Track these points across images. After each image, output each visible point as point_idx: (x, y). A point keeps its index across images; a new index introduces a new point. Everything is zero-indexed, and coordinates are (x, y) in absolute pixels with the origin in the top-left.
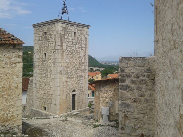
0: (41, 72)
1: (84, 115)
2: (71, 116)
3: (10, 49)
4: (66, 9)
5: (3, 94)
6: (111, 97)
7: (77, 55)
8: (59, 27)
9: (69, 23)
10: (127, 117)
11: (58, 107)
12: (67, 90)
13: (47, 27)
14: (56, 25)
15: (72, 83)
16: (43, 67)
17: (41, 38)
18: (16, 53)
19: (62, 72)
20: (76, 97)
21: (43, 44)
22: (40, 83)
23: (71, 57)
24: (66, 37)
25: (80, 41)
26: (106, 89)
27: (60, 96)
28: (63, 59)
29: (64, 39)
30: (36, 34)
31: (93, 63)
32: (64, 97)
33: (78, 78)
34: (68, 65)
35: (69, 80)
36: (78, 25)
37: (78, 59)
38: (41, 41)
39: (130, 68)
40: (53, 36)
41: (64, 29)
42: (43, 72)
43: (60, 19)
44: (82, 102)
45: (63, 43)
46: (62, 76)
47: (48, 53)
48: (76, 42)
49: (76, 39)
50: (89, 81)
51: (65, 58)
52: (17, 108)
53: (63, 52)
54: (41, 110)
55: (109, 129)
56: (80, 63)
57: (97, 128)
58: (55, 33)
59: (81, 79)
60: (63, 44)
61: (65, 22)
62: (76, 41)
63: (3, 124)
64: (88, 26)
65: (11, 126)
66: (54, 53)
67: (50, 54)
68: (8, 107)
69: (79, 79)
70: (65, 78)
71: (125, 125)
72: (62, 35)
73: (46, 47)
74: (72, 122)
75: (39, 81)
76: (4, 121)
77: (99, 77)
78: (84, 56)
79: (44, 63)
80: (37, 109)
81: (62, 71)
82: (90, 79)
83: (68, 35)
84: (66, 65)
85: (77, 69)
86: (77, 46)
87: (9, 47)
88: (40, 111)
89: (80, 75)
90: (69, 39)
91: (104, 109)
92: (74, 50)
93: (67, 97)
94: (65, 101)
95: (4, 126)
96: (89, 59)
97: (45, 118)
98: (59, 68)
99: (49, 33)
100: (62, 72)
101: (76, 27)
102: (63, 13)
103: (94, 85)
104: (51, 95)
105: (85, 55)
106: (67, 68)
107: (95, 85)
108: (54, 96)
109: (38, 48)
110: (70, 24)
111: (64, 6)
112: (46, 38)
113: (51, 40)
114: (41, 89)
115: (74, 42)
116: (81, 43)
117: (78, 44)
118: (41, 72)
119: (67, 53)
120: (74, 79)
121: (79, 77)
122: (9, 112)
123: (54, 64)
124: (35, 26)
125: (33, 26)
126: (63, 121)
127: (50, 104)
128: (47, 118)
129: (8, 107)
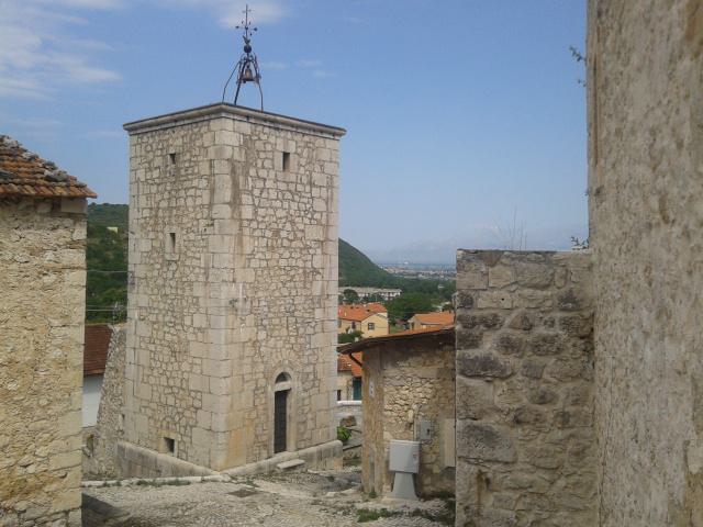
7: (295, 238)
13: (182, 133)
15: (275, 347)
16: (164, 286)
17: (156, 174)
20: (291, 401)
22: (152, 347)
24: (252, 172)
28: (242, 255)
35: (262, 335)
38: (159, 185)
40: (204, 169)
44: (314, 419)
48: (290, 191)
51: (248, 250)
56: (304, 272)
60: (240, 199)
66: (207, 232)
69: (301, 331)
70: (249, 329)
73: (178, 208)
83: (260, 165)
85: (294, 293)
86: (294, 206)
92: (284, 220)
95: (14, 510)
99: (188, 157)
104: (193, 394)
113: (195, 183)
115: (281, 191)
120: (284, 332)
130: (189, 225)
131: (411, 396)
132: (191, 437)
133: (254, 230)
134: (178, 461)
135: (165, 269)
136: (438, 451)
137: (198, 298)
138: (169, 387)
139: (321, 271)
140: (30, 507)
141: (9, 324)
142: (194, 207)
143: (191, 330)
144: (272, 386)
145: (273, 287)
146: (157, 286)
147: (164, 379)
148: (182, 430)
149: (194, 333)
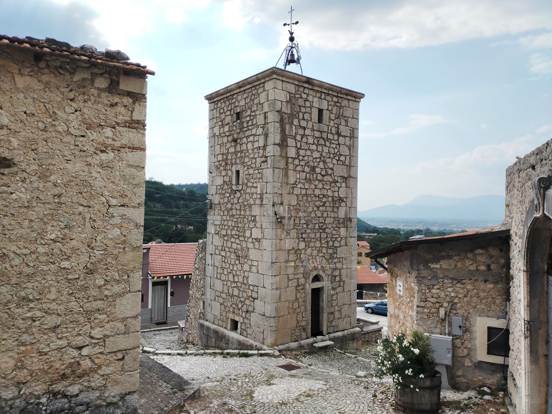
0: (226, 223)
7: (327, 174)
12: (297, 274)
13: (245, 96)
15: (311, 255)
16: (231, 209)
17: (226, 128)
19: (283, 221)
20: (325, 297)
22: (223, 253)
24: (296, 122)
28: (288, 184)
29: (291, 127)
30: (215, 120)
32: (290, 294)
34: (301, 203)
35: (302, 245)
37: (328, 187)
38: (228, 136)
40: (260, 120)
42: (232, 221)
44: (340, 311)
45: (289, 140)
46: (285, 233)
47: (246, 168)
48: (323, 139)
51: (292, 180)
52: (120, 326)
56: (333, 200)
59: (337, 244)
60: (287, 142)
66: (262, 167)
67: (251, 171)
69: (331, 243)
70: (292, 240)
72: (287, 116)
73: (241, 152)
75: (220, 248)
79: (234, 197)
83: (301, 117)
84: (294, 202)
85: (325, 215)
86: (326, 150)
88: (222, 330)
89: (334, 232)
92: (318, 160)
93: (299, 295)
94: (291, 306)
95: (65, 396)
99: (249, 112)
104: (251, 288)
111: (290, 44)
113: (254, 132)
114: (225, 271)
115: (316, 138)
116: (337, 142)
117: (328, 144)
118: (226, 223)
119: (299, 168)
120: (318, 244)
122: (88, 341)
130: (250, 163)
131: (442, 295)
132: (250, 320)
133: (297, 166)
134: (241, 338)
135: (232, 197)
136: (469, 346)
137: (255, 216)
138: (235, 282)
139: (345, 199)
140: (81, 391)
141: (63, 199)
142: (253, 150)
143: (250, 240)
144: (309, 284)
145: (310, 209)
146: (226, 209)
147: (231, 276)
148: (244, 314)
149: (253, 243)
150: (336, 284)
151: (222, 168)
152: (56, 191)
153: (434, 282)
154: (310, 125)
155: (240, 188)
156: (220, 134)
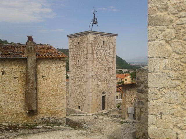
0: (75, 76)
1: (113, 115)
2: (101, 115)
3: (57, 61)
4: (95, 20)
5: (53, 94)
6: (135, 98)
8: (91, 38)
9: (99, 34)
10: (142, 111)
11: (90, 106)
14: (88, 36)
17: (75, 47)
18: (61, 64)
19: (93, 76)
20: (106, 98)
21: (77, 52)
22: (74, 86)
23: (101, 63)
24: (96, 46)
25: (109, 49)
26: (131, 91)
27: (92, 97)
28: (94, 65)
29: (95, 48)
31: (121, 64)
32: (96, 98)
33: (107, 82)
34: (98, 70)
35: (99, 83)
36: (106, 35)
38: (75, 49)
39: (143, 77)
40: (85, 46)
41: (95, 39)
43: (91, 31)
45: (94, 52)
48: (105, 50)
49: (105, 47)
50: (118, 83)
51: (95, 64)
52: (62, 105)
53: (94, 59)
54: (76, 108)
55: (134, 125)
57: (124, 124)
58: (87, 43)
59: (110, 82)
61: (95, 33)
62: (105, 49)
63: (53, 116)
64: (115, 35)
65: (58, 118)
67: (83, 61)
68: (56, 104)
69: (108, 82)
71: (140, 117)
73: (80, 54)
74: (103, 119)
75: (73, 84)
76: (53, 114)
77: (128, 80)
78: (112, 62)
80: (73, 108)
81: (93, 75)
82: (119, 81)
84: (96, 70)
86: (106, 53)
87: (57, 59)
88: (75, 109)
90: (99, 47)
91: (130, 109)
92: (103, 57)
95: (54, 117)
96: (117, 61)
97: (80, 116)
98: (90, 72)
99: (82, 43)
100: (93, 76)
101: (104, 37)
102: (93, 23)
103: (121, 88)
105: (114, 61)
106: (97, 73)
107: (123, 87)
108: (87, 97)
109: (73, 55)
110: (99, 35)
112: (79, 47)
119: (97, 60)
120: (104, 82)
121: (108, 80)
123: (86, 69)
124: (70, 36)
125: (68, 37)
126: (95, 118)
127: (84, 103)
128: (81, 116)
129: (56, 104)
135: (77, 68)
142: (83, 54)
147: (77, 93)
150: (110, 94)
151: (73, 59)
152: (52, 81)
153: (130, 94)
154: (101, 46)
155: (79, 66)
156: (72, 48)
